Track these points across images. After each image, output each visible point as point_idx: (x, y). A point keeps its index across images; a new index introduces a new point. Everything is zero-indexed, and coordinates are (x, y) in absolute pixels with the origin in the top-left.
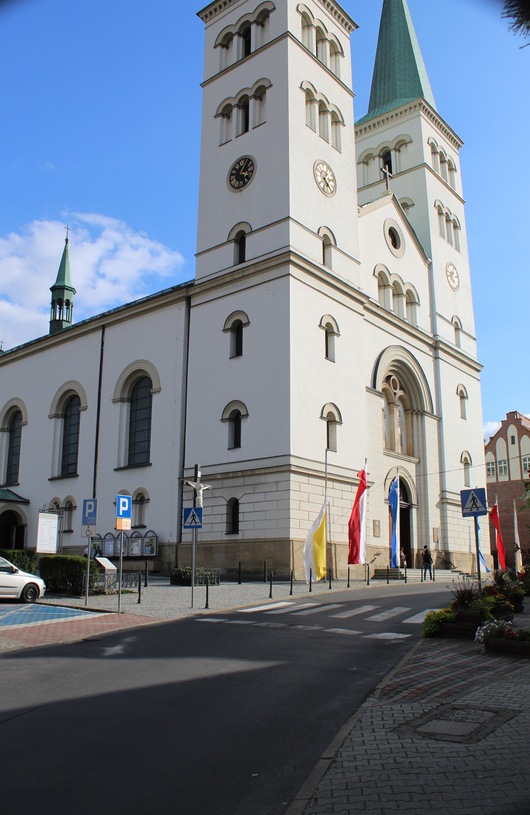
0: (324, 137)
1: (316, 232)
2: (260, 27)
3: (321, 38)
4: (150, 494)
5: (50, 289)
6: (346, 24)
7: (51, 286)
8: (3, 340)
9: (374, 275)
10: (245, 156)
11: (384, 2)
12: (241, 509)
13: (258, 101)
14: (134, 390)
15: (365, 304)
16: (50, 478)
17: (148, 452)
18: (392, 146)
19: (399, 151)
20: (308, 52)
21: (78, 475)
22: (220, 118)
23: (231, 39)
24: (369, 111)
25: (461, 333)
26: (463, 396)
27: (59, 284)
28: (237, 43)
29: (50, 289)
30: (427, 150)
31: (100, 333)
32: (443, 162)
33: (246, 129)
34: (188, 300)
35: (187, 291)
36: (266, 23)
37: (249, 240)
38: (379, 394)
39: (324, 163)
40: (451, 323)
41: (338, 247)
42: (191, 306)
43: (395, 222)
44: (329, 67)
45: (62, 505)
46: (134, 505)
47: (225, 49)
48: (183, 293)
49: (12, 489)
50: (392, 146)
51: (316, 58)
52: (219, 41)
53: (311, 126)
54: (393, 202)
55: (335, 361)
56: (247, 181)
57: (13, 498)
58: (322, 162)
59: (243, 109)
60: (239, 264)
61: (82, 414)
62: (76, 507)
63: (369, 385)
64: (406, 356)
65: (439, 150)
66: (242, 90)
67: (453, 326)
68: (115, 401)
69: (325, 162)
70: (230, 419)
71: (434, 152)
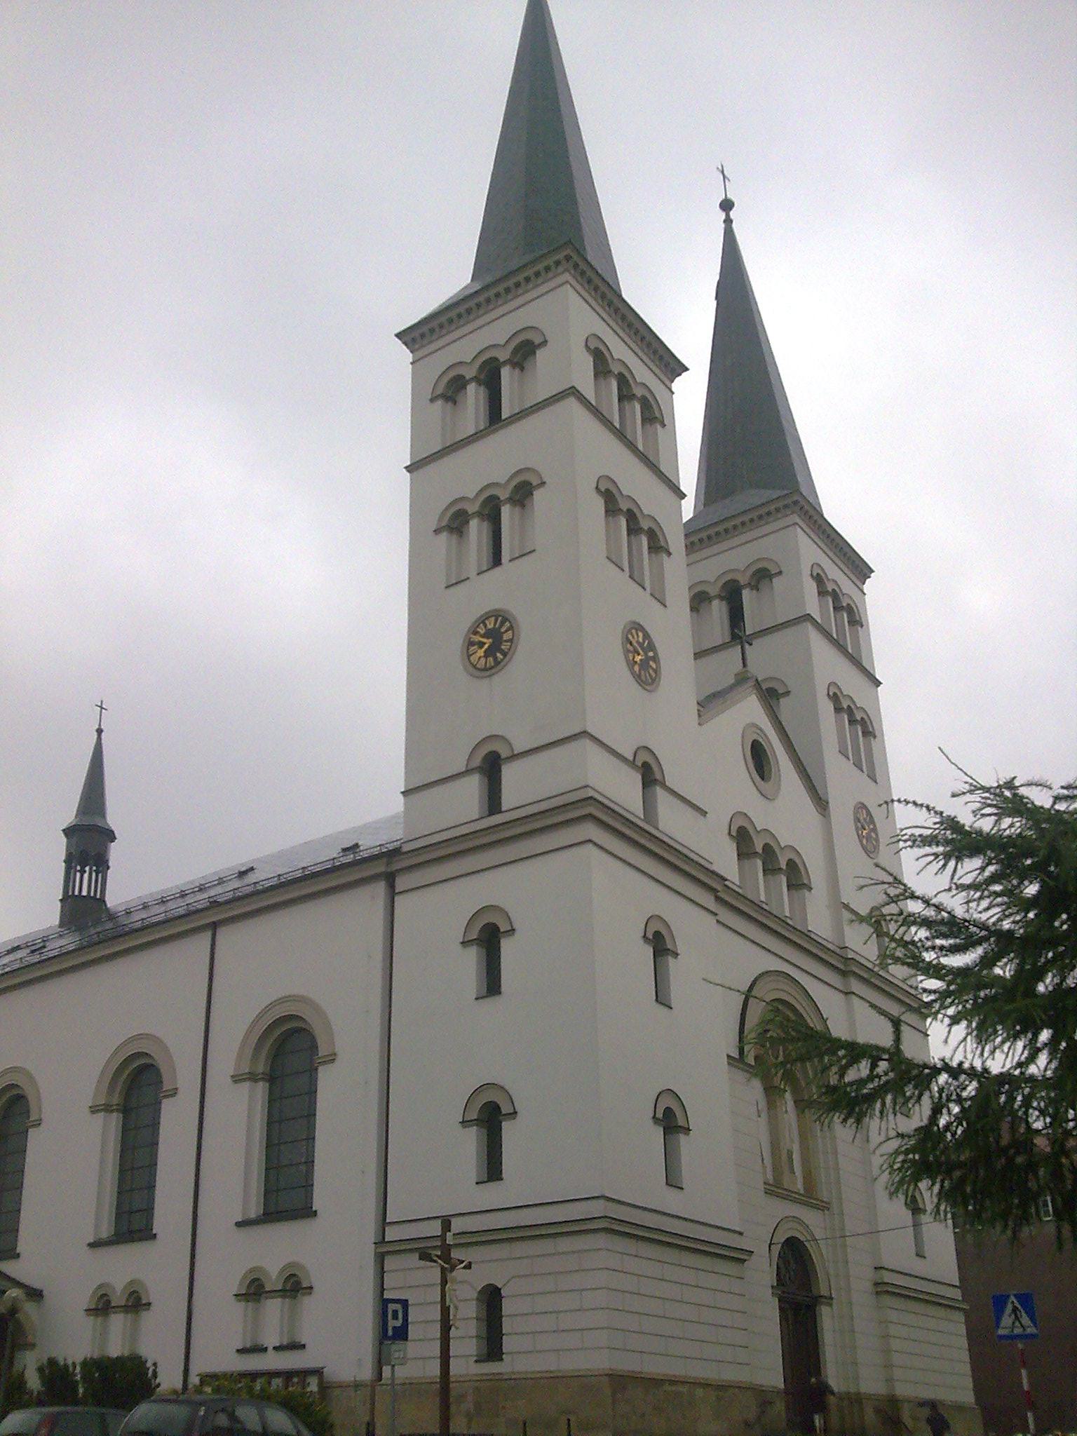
1: (631, 758)
2: (517, 371)
3: (625, 395)
4: (316, 1276)
5: (64, 830)
6: (643, 339)
12: (507, 1307)
16: (92, 1241)
17: (308, 1186)
18: (743, 580)
19: (522, 369)
20: (606, 422)
23: (464, 387)
24: (472, 280)
27: (87, 821)
28: (474, 396)
29: (64, 830)
30: (811, 587)
31: (204, 939)
33: (496, 560)
34: (390, 879)
35: (388, 864)
36: (527, 365)
37: (510, 775)
40: (632, 764)
42: (397, 891)
43: (761, 730)
44: (641, 448)
45: (118, 1299)
46: (279, 1300)
48: (380, 868)
50: (503, 355)
51: (620, 434)
52: (440, 391)
56: (502, 657)
58: (637, 626)
60: (489, 816)
61: (165, 1103)
63: (735, 1054)
65: (830, 587)
66: (488, 486)
67: (637, 771)
68: (237, 1079)
70: (478, 1122)
71: (822, 593)
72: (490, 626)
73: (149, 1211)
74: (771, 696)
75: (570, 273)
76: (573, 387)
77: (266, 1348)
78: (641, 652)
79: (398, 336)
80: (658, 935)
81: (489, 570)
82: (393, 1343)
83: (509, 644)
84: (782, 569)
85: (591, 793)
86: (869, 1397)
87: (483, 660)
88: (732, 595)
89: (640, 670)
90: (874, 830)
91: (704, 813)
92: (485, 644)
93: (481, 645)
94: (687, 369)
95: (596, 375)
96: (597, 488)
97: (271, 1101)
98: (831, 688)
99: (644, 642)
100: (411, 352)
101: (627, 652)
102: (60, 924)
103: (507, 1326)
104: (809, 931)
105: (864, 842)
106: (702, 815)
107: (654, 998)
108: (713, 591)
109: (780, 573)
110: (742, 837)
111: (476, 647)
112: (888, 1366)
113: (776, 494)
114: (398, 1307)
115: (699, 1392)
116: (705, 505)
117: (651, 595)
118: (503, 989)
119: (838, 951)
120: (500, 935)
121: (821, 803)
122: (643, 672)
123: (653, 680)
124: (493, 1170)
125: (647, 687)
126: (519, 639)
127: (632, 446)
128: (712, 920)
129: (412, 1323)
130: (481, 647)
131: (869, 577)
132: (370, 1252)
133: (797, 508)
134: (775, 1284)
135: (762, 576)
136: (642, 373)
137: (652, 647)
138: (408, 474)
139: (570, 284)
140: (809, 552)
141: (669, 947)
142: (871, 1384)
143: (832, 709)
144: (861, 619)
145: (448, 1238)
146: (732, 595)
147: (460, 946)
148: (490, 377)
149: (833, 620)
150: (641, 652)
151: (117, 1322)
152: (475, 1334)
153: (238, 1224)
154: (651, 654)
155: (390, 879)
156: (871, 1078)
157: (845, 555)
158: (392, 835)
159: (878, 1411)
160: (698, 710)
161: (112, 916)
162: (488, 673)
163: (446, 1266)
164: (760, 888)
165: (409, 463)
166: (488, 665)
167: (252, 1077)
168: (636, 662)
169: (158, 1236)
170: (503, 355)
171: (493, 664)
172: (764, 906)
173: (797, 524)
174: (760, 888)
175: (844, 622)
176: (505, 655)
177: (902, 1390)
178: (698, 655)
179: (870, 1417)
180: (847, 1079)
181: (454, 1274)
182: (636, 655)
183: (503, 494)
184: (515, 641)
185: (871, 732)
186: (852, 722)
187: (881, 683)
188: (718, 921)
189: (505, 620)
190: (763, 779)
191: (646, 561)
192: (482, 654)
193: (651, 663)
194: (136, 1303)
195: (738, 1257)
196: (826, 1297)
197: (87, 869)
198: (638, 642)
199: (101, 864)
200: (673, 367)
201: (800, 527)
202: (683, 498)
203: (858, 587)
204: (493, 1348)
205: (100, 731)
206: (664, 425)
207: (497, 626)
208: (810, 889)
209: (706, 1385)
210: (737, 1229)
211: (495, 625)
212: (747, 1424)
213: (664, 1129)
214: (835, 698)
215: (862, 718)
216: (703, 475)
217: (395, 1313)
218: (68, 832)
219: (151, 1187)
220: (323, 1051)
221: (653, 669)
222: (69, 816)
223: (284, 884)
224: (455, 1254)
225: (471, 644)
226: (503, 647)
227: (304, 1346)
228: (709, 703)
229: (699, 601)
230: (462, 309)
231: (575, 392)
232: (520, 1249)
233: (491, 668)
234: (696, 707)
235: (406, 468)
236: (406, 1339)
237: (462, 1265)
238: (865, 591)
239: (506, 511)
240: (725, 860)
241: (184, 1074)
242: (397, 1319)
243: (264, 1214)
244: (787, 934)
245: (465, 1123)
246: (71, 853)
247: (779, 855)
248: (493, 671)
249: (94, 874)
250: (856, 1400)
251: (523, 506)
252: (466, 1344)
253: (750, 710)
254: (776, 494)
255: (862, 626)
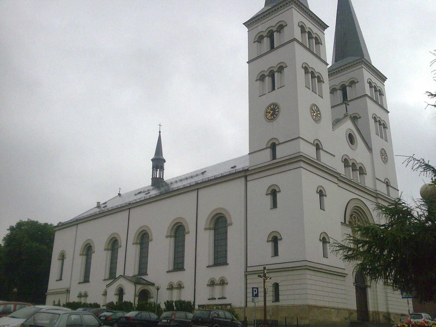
0: (314, 91)
3: (310, 37)
4: (229, 280)
5: (151, 160)
7: (151, 159)
8: (121, 188)
9: (342, 161)
10: (274, 103)
11: (338, 1)
12: (280, 288)
13: (279, 73)
14: (216, 223)
15: (338, 178)
19: (351, 87)
20: (305, 47)
21: (185, 269)
22: (259, 81)
25: (390, 188)
26: (321, 194)
28: (266, 41)
29: (151, 160)
30: (367, 86)
32: (376, 91)
33: (273, 89)
34: (246, 177)
36: (281, 31)
37: (278, 148)
38: (347, 225)
39: (315, 105)
40: (313, 144)
41: (323, 149)
42: (248, 180)
45: (175, 286)
47: (259, 43)
48: (243, 174)
49: (144, 277)
50: (274, 29)
51: (309, 50)
53: (377, 134)
54: (350, 119)
55: (324, 209)
57: (145, 282)
58: (314, 105)
59: (271, 77)
62: (184, 287)
64: (360, 203)
68: (206, 229)
69: (315, 105)
70: (271, 241)
71: (371, 87)
72: (272, 107)
73: (183, 263)
74: (354, 119)
75: (293, 5)
76: (295, 38)
77: (216, 299)
78: (316, 113)
79: (243, 24)
80: (321, 191)
81: (271, 91)
82: (255, 297)
83: (278, 112)
84: (358, 81)
85: (301, 154)
86: (382, 313)
87: (270, 117)
88: (344, 89)
89: (315, 117)
90: (387, 156)
91: (334, 156)
92: (271, 112)
93: (270, 113)
94: (329, 27)
95: (301, 33)
96: (302, 67)
97: (215, 235)
98: (373, 116)
99: (316, 109)
100: (248, 28)
101: (311, 113)
102: (152, 185)
103: (280, 293)
104: (366, 186)
105: (383, 159)
106: (333, 156)
107: (320, 208)
108: (338, 88)
109: (358, 82)
110: (346, 162)
111: (268, 113)
112: (387, 304)
113: (357, 58)
114: (256, 289)
115: (333, 310)
116: (335, 62)
117: (319, 95)
118: (278, 206)
119: (374, 191)
120: (276, 192)
121: (370, 149)
122: (316, 118)
123: (319, 120)
124: (276, 253)
125: (317, 122)
126: (280, 110)
127: (313, 53)
128: (337, 185)
129: (260, 292)
130: (269, 113)
131: (386, 80)
132: (243, 274)
133: (362, 62)
134: (354, 282)
135: (353, 83)
136: (315, 30)
137: (319, 110)
138: (248, 64)
139: (294, 8)
140: (367, 75)
141: (324, 194)
142: (382, 309)
143: (374, 121)
144: (383, 94)
145: (265, 272)
146: (344, 89)
147: (266, 195)
148: (271, 35)
149: (374, 94)
150: (316, 113)
151: (175, 292)
152: (272, 295)
153: (207, 267)
154: (318, 112)
155: (246, 177)
156: (353, 254)
157: (378, 75)
158: (246, 164)
159: (384, 316)
160: (333, 127)
161: (167, 184)
162: (272, 120)
163: (265, 278)
164: (351, 175)
165: (248, 61)
166: (272, 119)
167: (210, 229)
168: (314, 115)
169: (185, 270)
170: (274, 29)
171: (273, 118)
172: (352, 181)
173: (363, 67)
174: (351, 175)
175: (378, 95)
176: (276, 115)
177: (391, 311)
178: (332, 107)
179: (381, 317)
180: (348, 254)
181: (267, 280)
182: (314, 113)
183: (275, 70)
184: (279, 112)
185: (386, 127)
186: (380, 124)
187: (389, 112)
188: (338, 186)
189: (276, 106)
190: (352, 144)
191: (317, 85)
192: (270, 115)
193: (318, 115)
194: (180, 287)
195: (344, 275)
196: (369, 286)
197: (158, 170)
198: (315, 109)
199: (162, 168)
200: (324, 26)
201: (364, 68)
202: (328, 65)
203: (382, 84)
204: (277, 298)
205: (160, 132)
206: (322, 44)
207: (274, 107)
208: (366, 174)
209: (334, 308)
210: (344, 268)
211: (273, 107)
212: (346, 319)
213: (323, 242)
214: (375, 118)
215: (383, 123)
216: (334, 53)
217: (255, 291)
218: (152, 160)
219: (183, 257)
220: (229, 222)
221: (319, 116)
222: (153, 156)
223: (216, 179)
224: (267, 275)
225: (267, 112)
226: (276, 113)
227: (226, 298)
228: (336, 122)
229: (333, 91)
230: (262, 16)
231: (296, 39)
232: (284, 274)
233: (273, 119)
234: (332, 126)
235: (247, 62)
236: (258, 297)
237: (269, 278)
238: (385, 85)
239: (276, 74)
240: (340, 169)
241: (191, 227)
242: (256, 292)
243: (214, 264)
244: (359, 188)
245: (268, 241)
246: (154, 166)
247: (357, 166)
248: (273, 120)
249: (160, 172)
250: (377, 313)
251: (281, 73)
252: (270, 297)
253: (348, 125)
254: (357, 58)
255: (383, 95)
